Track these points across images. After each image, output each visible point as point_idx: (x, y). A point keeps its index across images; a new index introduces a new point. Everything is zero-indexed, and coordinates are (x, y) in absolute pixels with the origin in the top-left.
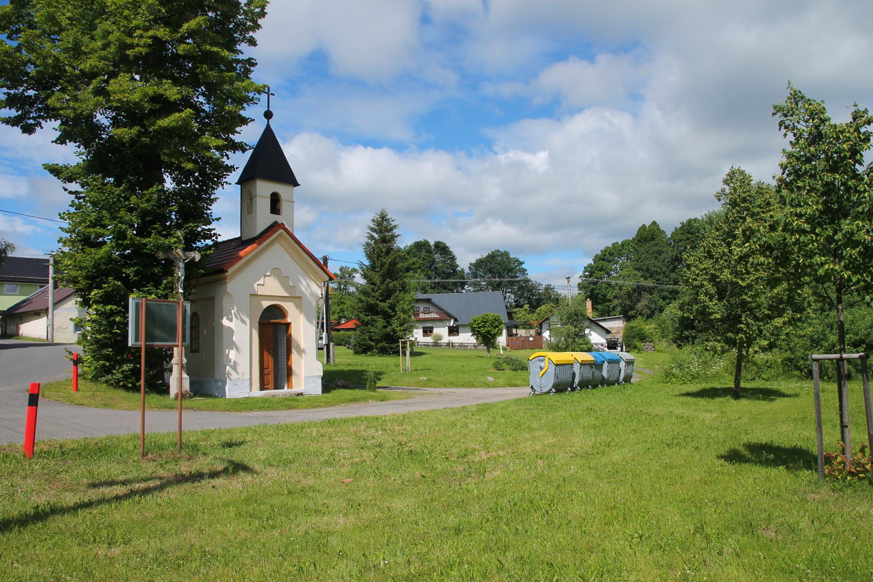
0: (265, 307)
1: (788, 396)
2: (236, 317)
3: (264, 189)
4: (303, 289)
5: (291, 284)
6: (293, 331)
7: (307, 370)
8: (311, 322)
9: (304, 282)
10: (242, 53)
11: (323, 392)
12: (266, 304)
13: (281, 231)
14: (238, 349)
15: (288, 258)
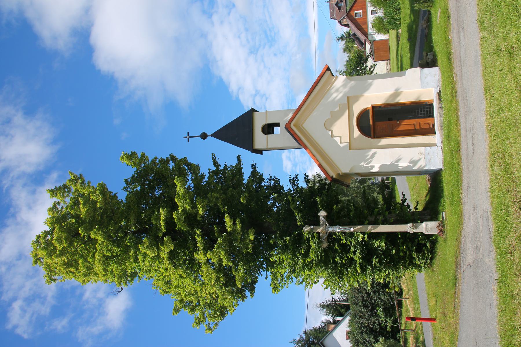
0: (359, 133)
1: (421, 75)
2: (370, 162)
3: (260, 139)
4: (341, 95)
5: (337, 109)
6: (379, 102)
7: (417, 85)
8: (370, 85)
10: (252, 295)
11: (437, 66)
12: (357, 133)
13: (292, 126)
14: (398, 161)
15: (314, 113)
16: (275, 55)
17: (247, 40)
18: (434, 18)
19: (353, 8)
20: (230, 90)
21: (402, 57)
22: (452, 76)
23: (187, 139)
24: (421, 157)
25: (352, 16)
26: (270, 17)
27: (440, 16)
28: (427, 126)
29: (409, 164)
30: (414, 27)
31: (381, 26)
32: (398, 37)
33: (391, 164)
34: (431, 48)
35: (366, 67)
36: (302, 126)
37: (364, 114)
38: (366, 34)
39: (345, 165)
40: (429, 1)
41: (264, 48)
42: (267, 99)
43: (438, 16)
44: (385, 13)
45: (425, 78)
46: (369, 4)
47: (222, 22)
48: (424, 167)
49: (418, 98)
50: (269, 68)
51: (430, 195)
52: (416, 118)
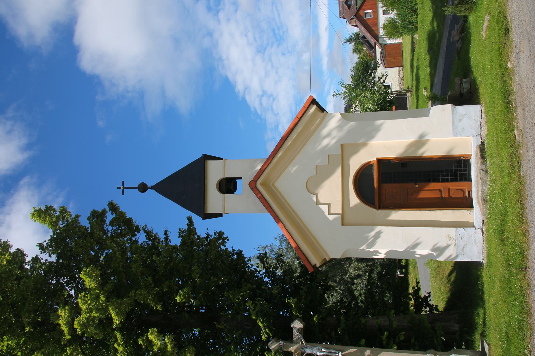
3: (215, 200)
4: (334, 141)
7: (446, 130)
8: (377, 129)
9: (325, 142)
11: (478, 103)
12: (354, 200)
14: (416, 245)
16: (283, 54)
17: (255, 39)
18: (473, 29)
19: (363, 8)
20: (236, 90)
21: (418, 68)
22: (512, 131)
23: (121, 190)
24: (449, 243)
25: (361, 17)
26: (279, 15)
27: (487, 27)
28: (460, 195)
29: (430, 252)
30: (437, 35)
31: (393, 29)
32: (413, 43)
33: (406, 250)
34: (466, 71)
35: (375, 78)
36: (273, 185)
37: (364, 172)
38: (376, 37)
39: (335, 246)
40: (467, 3)
41: (272, 47)
42: (274, 100)
43: (485, 26)
44: (398, 15)
45: (460, 121)
46: (380, 5)
47: (228, 20)
48: (457, 256)
49: (450, 151)
50: (277, 68)
51: (457, 273)
52: (443, 181)
